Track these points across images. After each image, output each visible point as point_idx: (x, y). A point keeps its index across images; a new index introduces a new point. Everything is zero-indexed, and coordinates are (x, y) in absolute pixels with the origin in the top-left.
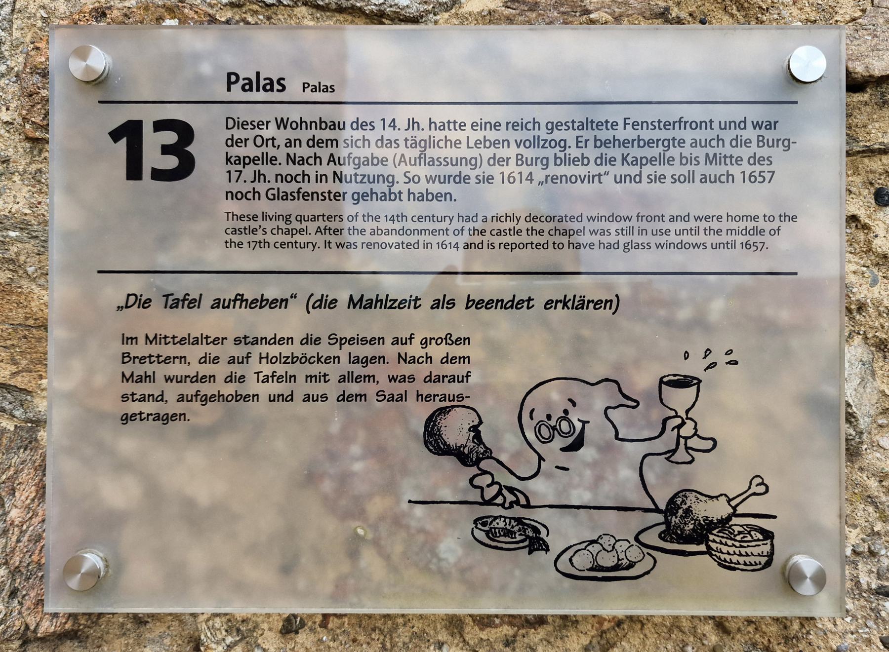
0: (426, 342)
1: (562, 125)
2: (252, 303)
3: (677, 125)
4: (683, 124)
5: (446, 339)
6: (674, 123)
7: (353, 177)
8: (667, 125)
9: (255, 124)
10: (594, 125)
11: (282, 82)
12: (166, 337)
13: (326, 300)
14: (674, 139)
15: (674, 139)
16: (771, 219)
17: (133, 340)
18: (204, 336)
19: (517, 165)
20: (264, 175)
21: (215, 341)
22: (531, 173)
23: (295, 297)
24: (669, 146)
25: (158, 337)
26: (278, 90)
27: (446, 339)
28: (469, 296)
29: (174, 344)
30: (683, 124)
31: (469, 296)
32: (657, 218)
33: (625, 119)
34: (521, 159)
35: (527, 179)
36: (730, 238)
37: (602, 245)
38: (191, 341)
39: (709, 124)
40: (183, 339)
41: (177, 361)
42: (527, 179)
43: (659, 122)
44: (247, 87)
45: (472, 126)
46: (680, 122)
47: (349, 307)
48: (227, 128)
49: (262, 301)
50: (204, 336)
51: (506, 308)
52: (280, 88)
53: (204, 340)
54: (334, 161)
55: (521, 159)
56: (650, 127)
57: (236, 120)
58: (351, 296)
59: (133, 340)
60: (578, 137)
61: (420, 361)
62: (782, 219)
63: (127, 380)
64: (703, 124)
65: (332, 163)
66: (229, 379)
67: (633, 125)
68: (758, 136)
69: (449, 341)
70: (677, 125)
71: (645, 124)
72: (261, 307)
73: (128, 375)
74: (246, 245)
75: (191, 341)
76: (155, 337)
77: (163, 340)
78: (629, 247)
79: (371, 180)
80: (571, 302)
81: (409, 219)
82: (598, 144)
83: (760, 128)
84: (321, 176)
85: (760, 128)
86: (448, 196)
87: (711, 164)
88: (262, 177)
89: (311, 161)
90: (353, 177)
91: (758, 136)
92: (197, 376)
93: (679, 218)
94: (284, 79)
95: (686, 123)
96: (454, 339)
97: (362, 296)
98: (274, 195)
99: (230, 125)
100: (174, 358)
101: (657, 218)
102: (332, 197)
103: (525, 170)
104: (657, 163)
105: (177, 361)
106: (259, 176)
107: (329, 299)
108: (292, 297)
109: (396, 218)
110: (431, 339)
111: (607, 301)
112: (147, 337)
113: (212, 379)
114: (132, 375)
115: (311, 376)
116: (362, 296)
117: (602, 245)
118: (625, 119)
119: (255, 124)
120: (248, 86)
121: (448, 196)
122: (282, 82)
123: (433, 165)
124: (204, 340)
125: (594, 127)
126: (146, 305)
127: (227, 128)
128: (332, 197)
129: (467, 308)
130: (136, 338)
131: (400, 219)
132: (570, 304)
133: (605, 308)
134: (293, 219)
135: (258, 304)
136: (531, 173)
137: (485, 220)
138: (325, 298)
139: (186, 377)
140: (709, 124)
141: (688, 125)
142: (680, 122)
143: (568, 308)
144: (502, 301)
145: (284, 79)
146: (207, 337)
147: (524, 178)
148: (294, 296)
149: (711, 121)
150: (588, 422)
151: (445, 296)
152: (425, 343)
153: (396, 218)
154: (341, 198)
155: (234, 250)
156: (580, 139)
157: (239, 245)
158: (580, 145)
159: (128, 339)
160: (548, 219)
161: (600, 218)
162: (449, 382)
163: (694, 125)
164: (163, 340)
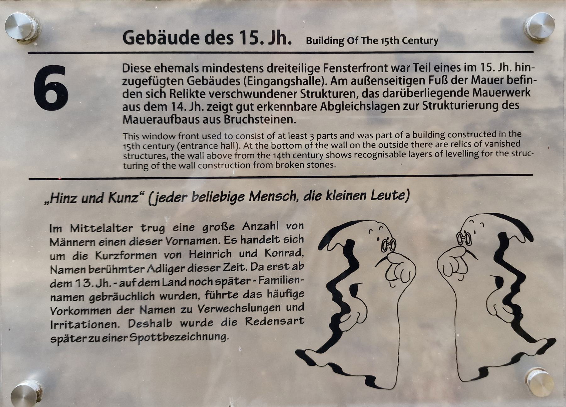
0: (207, 229)
1: (455, 68)
2: (355, 196)
3: (362, 68)
4: (366, 68)
5: (222, 226)
6: (422, 92)
7: (250, 106)
8: (169, 69)
9: (144, 68)
10: (291, 68)
11: (231, 37)
12: (86, 227)
13: (314, 194)
14: (168, 79)
15: (168, 79)
16: (230, 137)
17: (58, 229)
18: (116, 225)
19: (307, 43)
20: (199, 105)
21: (124, 229)
22: (181, 103)
23: (143, 194)
24: (164, 84)
25: (80, 226)
26: (228, 43)
27: (222, 226)
28: (194, 192)
29: (93, 231)
30: (366, 68)
31: (194, 192)
32: (193, 136)
33: (325, 64)
34: (228, 119)
35: (178, 108)
36: (182, 152)
37: (223, 146)
38: (106, 229)
39: (384, 68)
40: (99, 228)
41: (88, 243)
42: (178, 108)
43: (243, 66)
44: (354, 83)
45: (155, 69)
46: (364, 66)
47: (250, 200)
48: (124, 71)
49: (222, 196)
50: (116, 225)
51: (97, 202)
52: (229, 41)
53: (116, 229)
54: (335, 82)
55: (228, 119)
56: (343, 70)
57: (130, 65)
58: (252, 192)
59: (58, 229)
60: (430, 76)
61: (295, 241)
62: (284, 156)
63: (54, 245)
64: (380, 68)
65: (334, 84)
66: (76, 257)
67: (330, 69)
68: (171, 90)
69: (225, 228)
70: (362, 68)
71: (255, 68)
72: (221, 200)
73: (54, 241)
74: (510, 154)
75: (106, 229)
76: (78, 227)
77: (84, 229)
78: (377, 156)
79: (412, 107)
80: (332, 195)
81: (291, 156)
82: (510, 81)
83: (397, 71)
84: (526, 66)
85: (397, 71)
86: (290, 119)
87: (477, 95)
88: (198, 107)
89: (235, 95)
90: (250, 106)
91: (171, 90)
92: (183, 294)
93: (347, 136)
94: (232, 35)
95: (368, 67)
96: (228, 226)
97: (260, 191)
98: (193, 81)
99: (126, 69)
100: (86, 241)
101: (193, 136)
102: (351, 70)
103: (177, 101)
104: (182, 96)
105: (182, 242)
106: (195, 106)
107: (316, 194)
108: (140, 194)
109: (281, 156)
110: (211, 226)
111: (362, 194)
112: (72, 227)
113: (154, 256)
114: (57, 241)
115: (200, 239)
116: (260, 191)
117: (223, 146)
118: (325, 64)
119: (144, 68)
120: (139, 39)
121: (290, 119)
122: (231, 37)
123: (373, 97)
124: (116, 229)
125: (291, 70)
126: (318, 198)
127: (124, 71)
128: (351, 70)
129: (193, 201)
130: (60, 227)
131: (284, 156)
132: (332, 197)
133: (269, 200)
134: (446, 136)
135: (219, 198)
136: (181, 103)
137: (408, 136)
138: (313, 193)
139: (175, 295)
140: (384, 68)
141: (369, 68)
142: (364, 66)
143: (331, 199)
144: (94, 196)
145: (232, 35)
146: (118, 226)
147: (176, 106)
148: (142, 193)
149: (386, 66)
150: (133, 309)
151: (335, 190)
152: (206, 229)
153: (281, 156)
154: (185, 147)
155: (502, 158)
156: (250, 79)
157: (506, 154)
158: (250, 83)
159: (54, 228)
160: (454, 135)
161: (457, 135)
162: (290, 256)
163: (373, 69)
164: (84, 229)
